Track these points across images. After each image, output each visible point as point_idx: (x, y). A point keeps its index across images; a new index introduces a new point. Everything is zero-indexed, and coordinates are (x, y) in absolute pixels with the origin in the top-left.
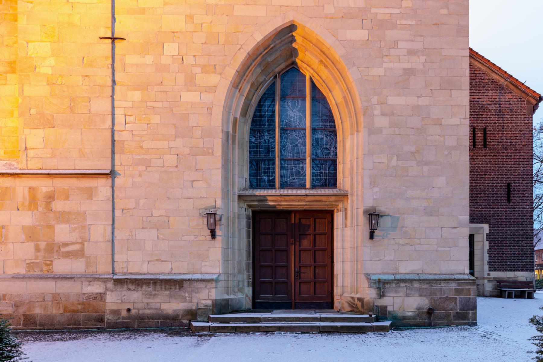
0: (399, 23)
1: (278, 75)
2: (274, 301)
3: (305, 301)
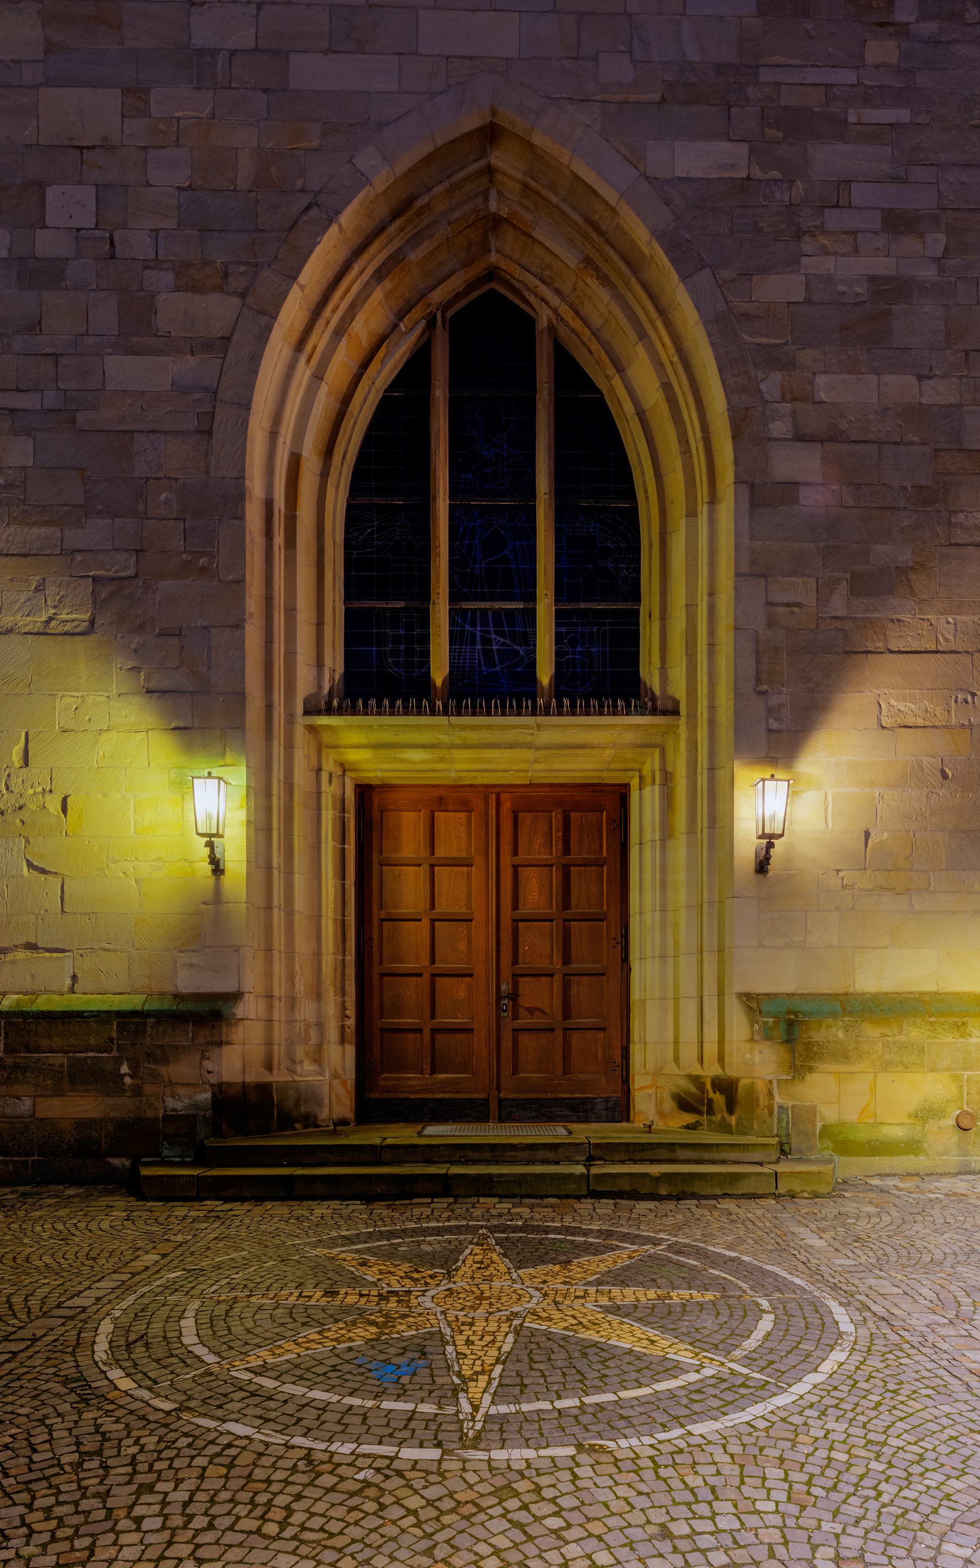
0: (855, 121)
1: (439, 314)
2: (429, 1096)
3: (535, 1096)
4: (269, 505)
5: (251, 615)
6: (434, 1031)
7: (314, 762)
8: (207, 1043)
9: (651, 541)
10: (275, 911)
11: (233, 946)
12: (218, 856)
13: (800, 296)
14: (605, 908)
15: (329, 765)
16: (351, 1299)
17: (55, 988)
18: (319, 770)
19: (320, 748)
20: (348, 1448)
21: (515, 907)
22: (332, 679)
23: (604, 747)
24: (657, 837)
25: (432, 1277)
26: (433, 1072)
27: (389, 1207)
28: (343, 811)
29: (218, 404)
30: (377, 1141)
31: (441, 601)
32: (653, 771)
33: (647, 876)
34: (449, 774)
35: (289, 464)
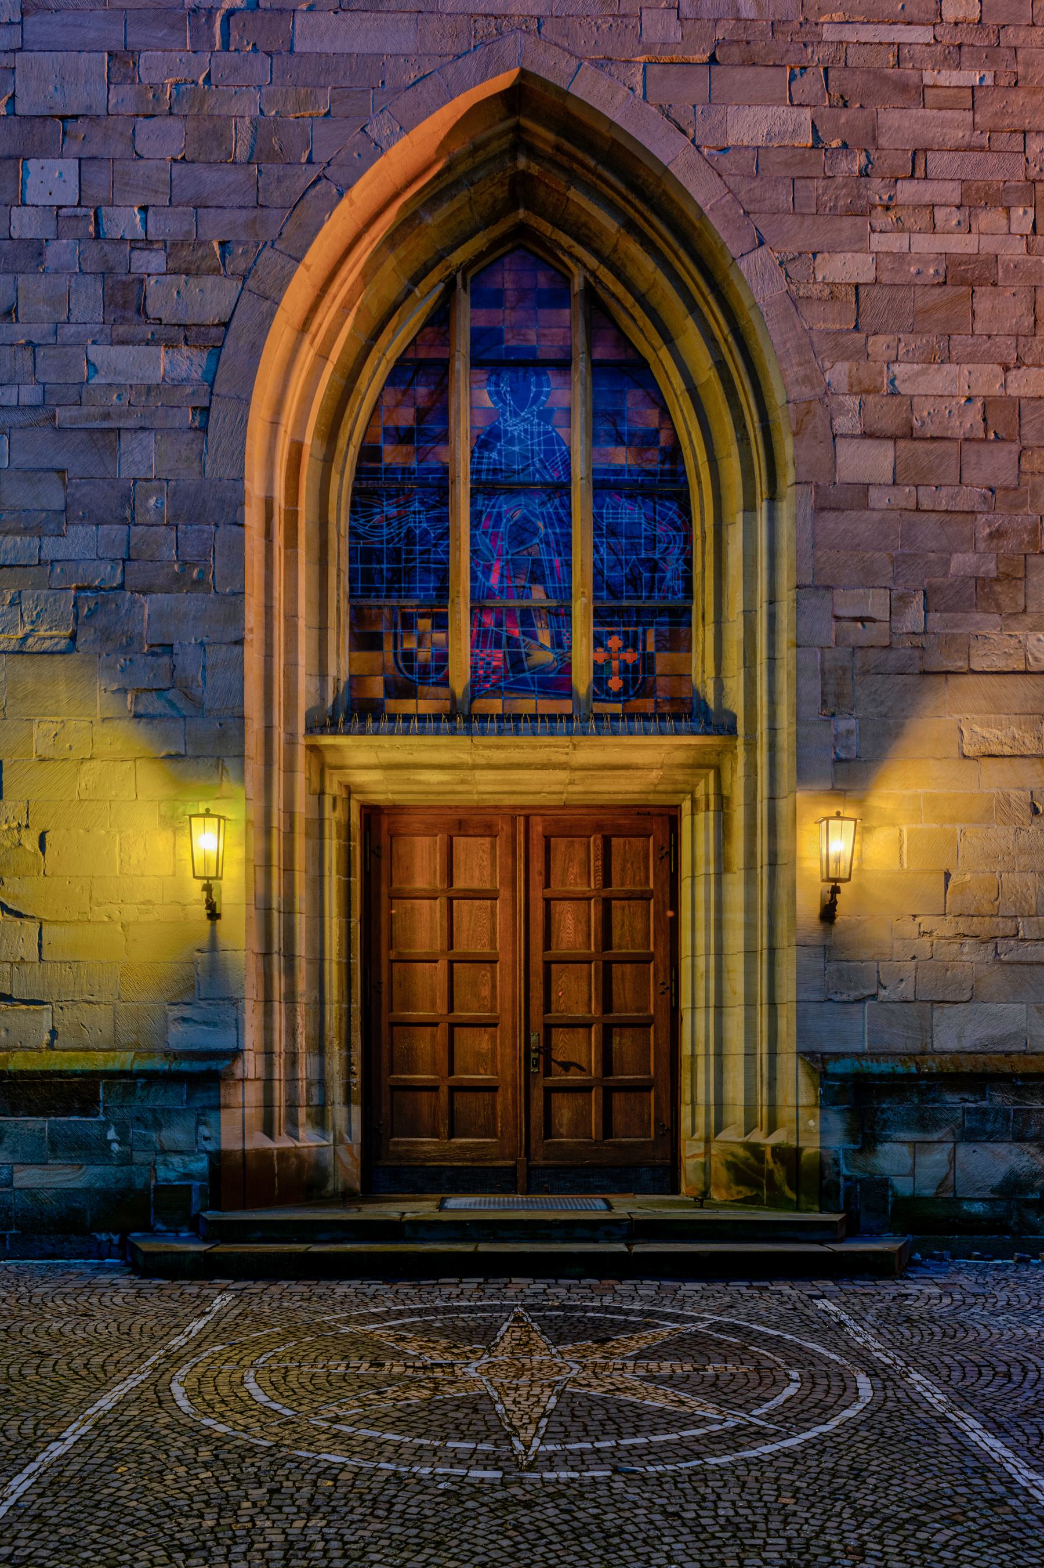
1: (459, 276)
4: (269, 503)
5: (251, 630)
6: (453, 1090)
7: (316, 785)
8: (203, 1107)
9: (703, 532)
10: (275, 957)
11: (229, 999)
12: (215, 898)
13: (868, 276)
14: (652, 949)
15: (333, 788)
16: (397, 1370)
17: (32, 1043)
18: (322, 793)
19: (322, 769)
20: (427, 1470)
21: (547, 946)
22: (337, 689)
23: (650, 768)
24: (712, 871)
25: (472, 1352)
26: (452, 1135)
27: (414, 1287)
28: (349, 838)
29: (214, 398)
30: (396, 1216)
31: (462, 600)
32: (707, 795)
33: (701, 914)
34: (470, 797)
35: (290, 454)
